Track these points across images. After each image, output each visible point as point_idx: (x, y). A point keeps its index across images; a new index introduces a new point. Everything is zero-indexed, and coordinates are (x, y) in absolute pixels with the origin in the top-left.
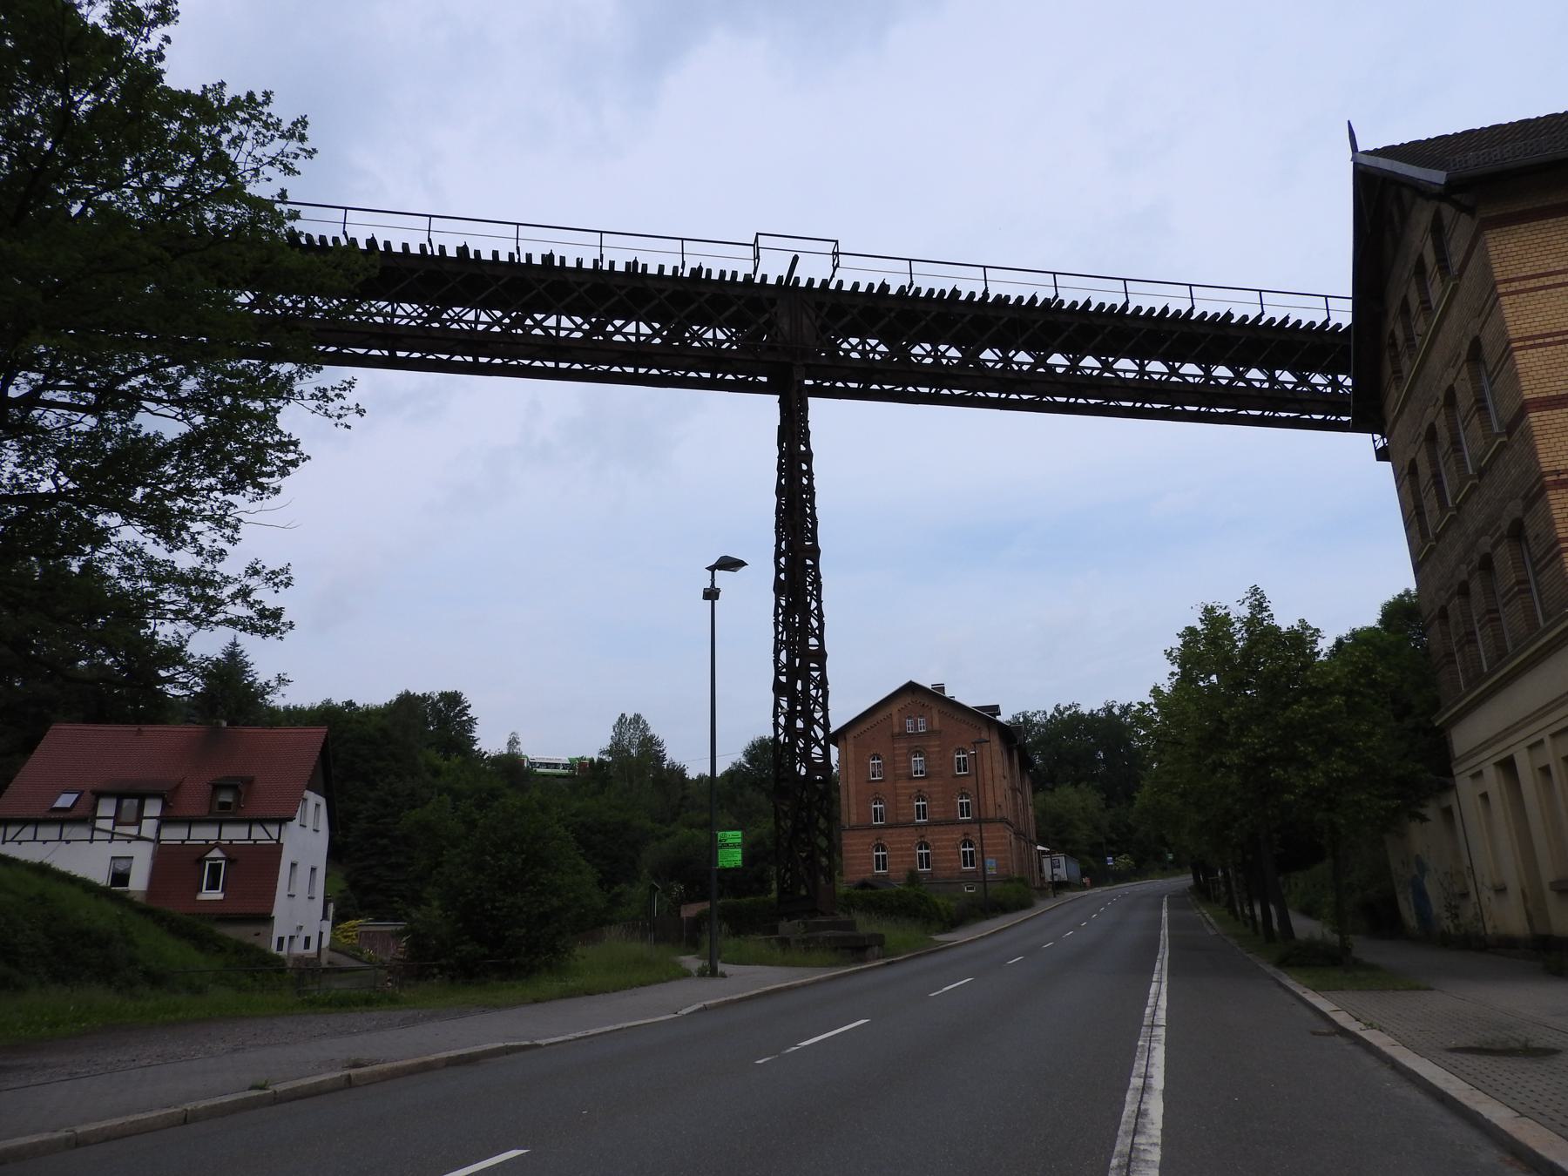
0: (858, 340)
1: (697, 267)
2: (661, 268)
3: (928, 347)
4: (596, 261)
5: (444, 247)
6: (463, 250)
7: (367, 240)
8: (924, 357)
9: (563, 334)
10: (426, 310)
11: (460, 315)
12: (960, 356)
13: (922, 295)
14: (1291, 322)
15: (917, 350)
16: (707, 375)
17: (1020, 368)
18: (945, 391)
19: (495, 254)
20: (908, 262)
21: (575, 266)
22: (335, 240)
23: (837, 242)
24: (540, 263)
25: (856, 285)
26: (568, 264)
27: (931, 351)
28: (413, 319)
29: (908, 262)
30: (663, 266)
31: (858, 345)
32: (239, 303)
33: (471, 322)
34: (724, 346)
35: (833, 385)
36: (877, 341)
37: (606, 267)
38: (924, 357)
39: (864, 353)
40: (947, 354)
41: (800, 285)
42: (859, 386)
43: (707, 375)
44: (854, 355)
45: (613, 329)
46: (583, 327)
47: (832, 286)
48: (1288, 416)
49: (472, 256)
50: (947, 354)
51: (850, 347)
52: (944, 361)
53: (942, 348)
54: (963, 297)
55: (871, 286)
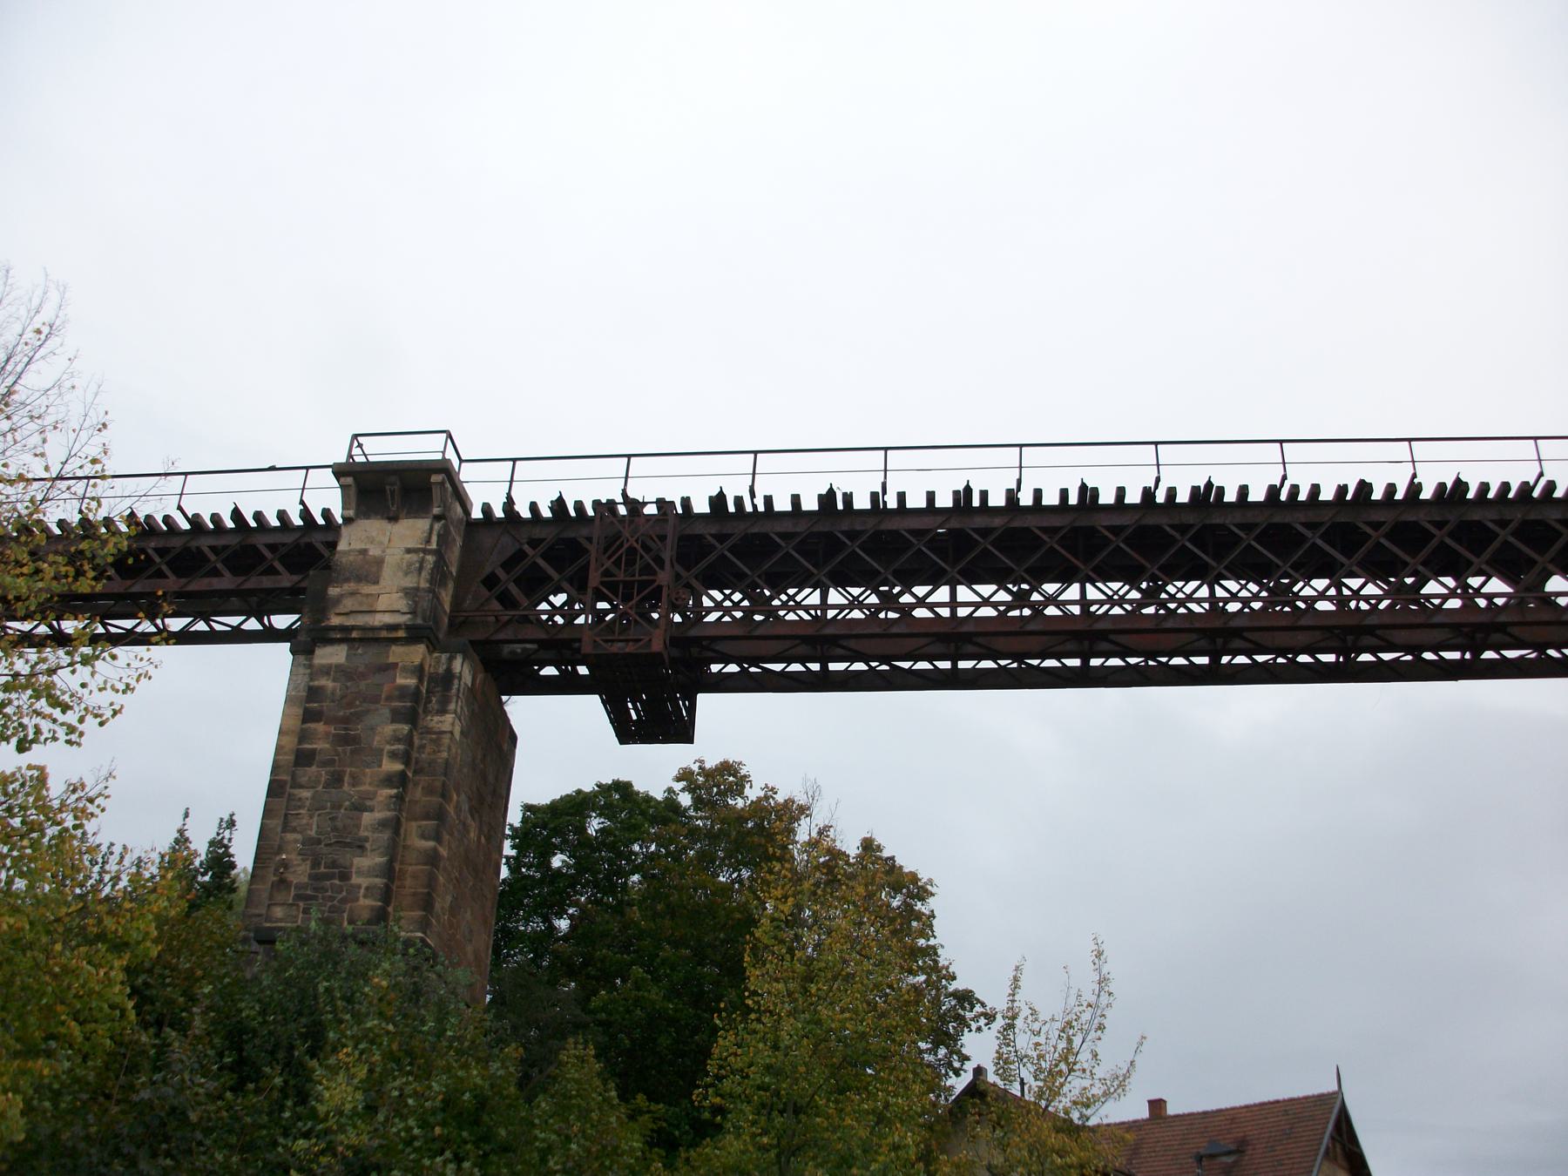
0: (1326, 582)
1: (961, 488)
2: (1121, 492)
3: (1450, 582)
4: (874, 496)
5: (798, 496)
6: (827, 499)
7: (820, 496)
8: (1445, 598)
9: (831, 614)
10: (1262, 587)
11: (861, 599)
12: (1510, 590)
13: (1302, 497)
15: (1432, 587)
16: (1203, 660)
17: (1374, 607)
18: (1489, 655)
19: (796, 500)
20: (752, 456)
21: (869, 507)
22: (739, 501)
24: (708, 511)
25: (1315, 489)
26: (939, 504)
27: (1456, 588)
28: (727, 611)
29: (1153, 446)
30: (1318, 485)
31: (1327, 588)
32: (1428, 597)
33: (815, 607)
34: (1382, 606)
35: (1293, 661)
36: (1363, 580)
37: (892, 503)
38: (1445, 598)
39: (1341, 601)
40: (1483, 590)
41: (1373, 498)
42: (1338, 658)
43: (1203, 660)
44: (1323, 606)
45: (730, 604)
46: (1178, 596)
47: (1160, 497)
48: (1522, 657)
49: (731, 508)
50: (1483, 590)
51: (914, 601)
52: (1482, 603)
53: (1475, 582)
54: (1377, 495)
55: (1342, 490)
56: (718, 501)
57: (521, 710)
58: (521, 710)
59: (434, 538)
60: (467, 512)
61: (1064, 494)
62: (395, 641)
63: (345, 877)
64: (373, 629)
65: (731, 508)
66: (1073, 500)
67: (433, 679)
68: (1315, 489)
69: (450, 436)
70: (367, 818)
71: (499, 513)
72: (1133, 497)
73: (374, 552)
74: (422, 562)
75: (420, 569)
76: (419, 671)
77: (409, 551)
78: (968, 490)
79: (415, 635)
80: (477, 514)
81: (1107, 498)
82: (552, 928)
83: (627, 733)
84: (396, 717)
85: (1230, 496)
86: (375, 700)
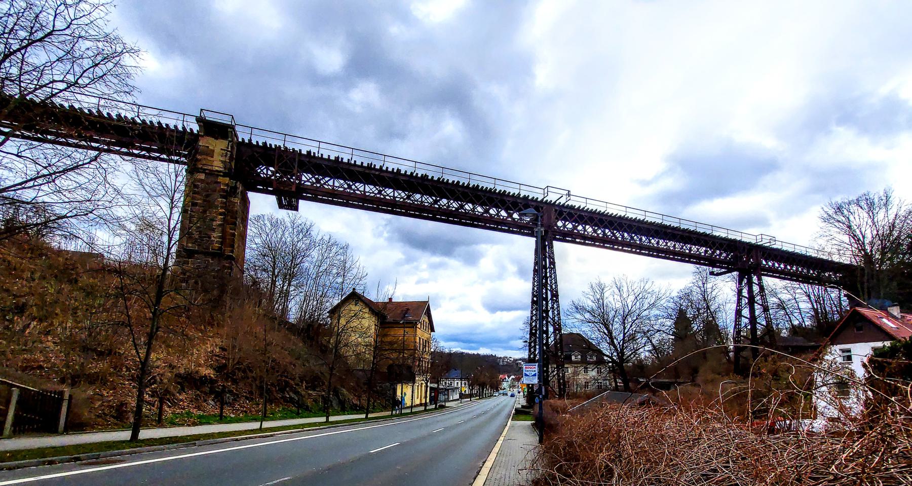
14: (598, 211)
22: (314, 153)
23: (569, 191)
37: (353, 162)
49: (312, 155)
55: (454, 181)
56: (309, 153)
57: (251, 195)
58: (251, 195)
59: (230, 147)
60: (238, 140)
61: (393, 169)
62: (220, 176)
63: (210, 238)
64: (213, 171)
65: (312, 155)
66: (395, 171)
67: (231, 188)
68: (448, 180)
69: (233, 117)
70: (214, 223)
71: (247, 141)
72: (409, 173)
73: (211, 148)
74: (226, 154)
75: (226, 156)
76: (227, 185)
77: (222, 149)
78: (371, 164)
79: (225, 175)
80: (240, 140)
81: (403, 172)
82: (88, 125)
83: (281, 206)
84: (222, 197)
85: (430, 178)
86: (215, 191)
